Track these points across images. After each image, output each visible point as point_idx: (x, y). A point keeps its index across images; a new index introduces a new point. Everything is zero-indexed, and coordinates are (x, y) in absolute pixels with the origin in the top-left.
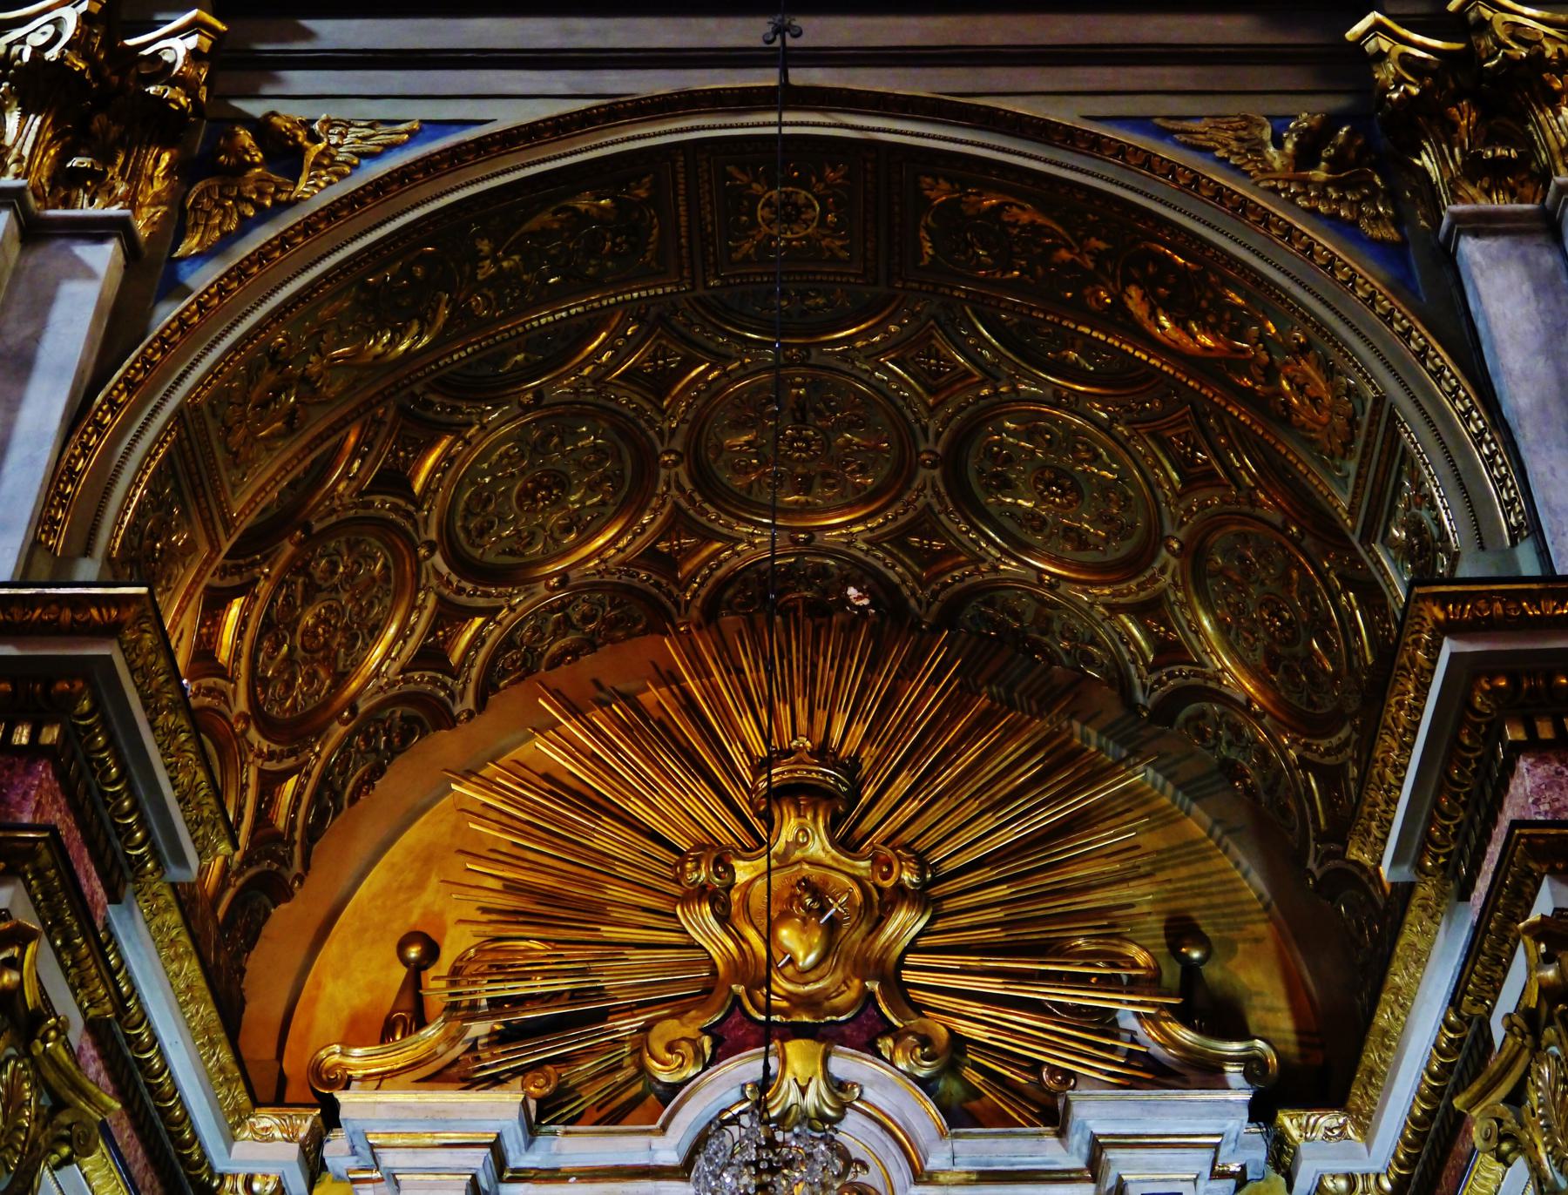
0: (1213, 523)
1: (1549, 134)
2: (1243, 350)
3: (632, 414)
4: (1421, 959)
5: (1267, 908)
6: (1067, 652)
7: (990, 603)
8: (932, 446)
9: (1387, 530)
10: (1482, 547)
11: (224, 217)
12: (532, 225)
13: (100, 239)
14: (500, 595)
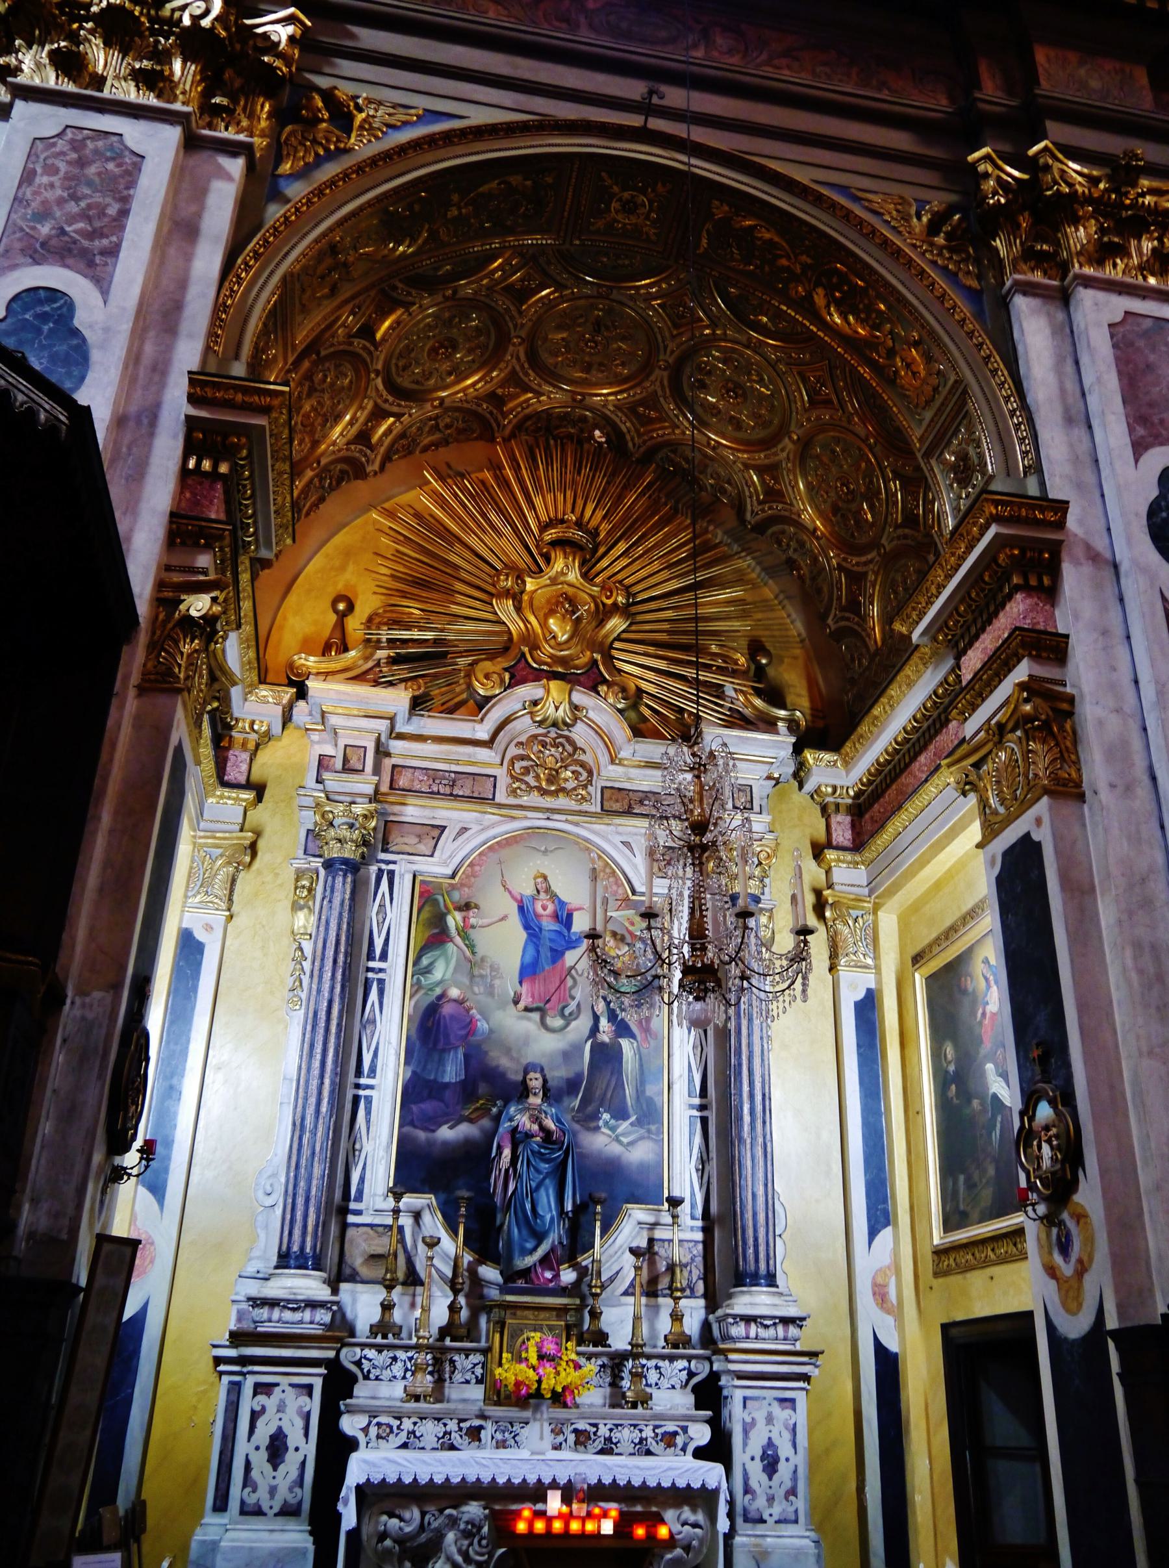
0: (822, 428)
1: (1071, 242)
2: (877, 337)
3: (502, 311)
4: (910, 685)
5: (802, 641)
6: (711, 485)
7: (674, 452)
8: (667, 358)
9: (942, 453)
10: (1008, 475)
11: (305, 152)
12: (483, 189)
13: (234, 155)
14: (406, 407)
